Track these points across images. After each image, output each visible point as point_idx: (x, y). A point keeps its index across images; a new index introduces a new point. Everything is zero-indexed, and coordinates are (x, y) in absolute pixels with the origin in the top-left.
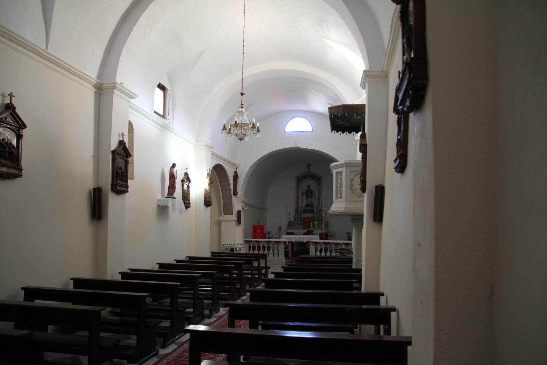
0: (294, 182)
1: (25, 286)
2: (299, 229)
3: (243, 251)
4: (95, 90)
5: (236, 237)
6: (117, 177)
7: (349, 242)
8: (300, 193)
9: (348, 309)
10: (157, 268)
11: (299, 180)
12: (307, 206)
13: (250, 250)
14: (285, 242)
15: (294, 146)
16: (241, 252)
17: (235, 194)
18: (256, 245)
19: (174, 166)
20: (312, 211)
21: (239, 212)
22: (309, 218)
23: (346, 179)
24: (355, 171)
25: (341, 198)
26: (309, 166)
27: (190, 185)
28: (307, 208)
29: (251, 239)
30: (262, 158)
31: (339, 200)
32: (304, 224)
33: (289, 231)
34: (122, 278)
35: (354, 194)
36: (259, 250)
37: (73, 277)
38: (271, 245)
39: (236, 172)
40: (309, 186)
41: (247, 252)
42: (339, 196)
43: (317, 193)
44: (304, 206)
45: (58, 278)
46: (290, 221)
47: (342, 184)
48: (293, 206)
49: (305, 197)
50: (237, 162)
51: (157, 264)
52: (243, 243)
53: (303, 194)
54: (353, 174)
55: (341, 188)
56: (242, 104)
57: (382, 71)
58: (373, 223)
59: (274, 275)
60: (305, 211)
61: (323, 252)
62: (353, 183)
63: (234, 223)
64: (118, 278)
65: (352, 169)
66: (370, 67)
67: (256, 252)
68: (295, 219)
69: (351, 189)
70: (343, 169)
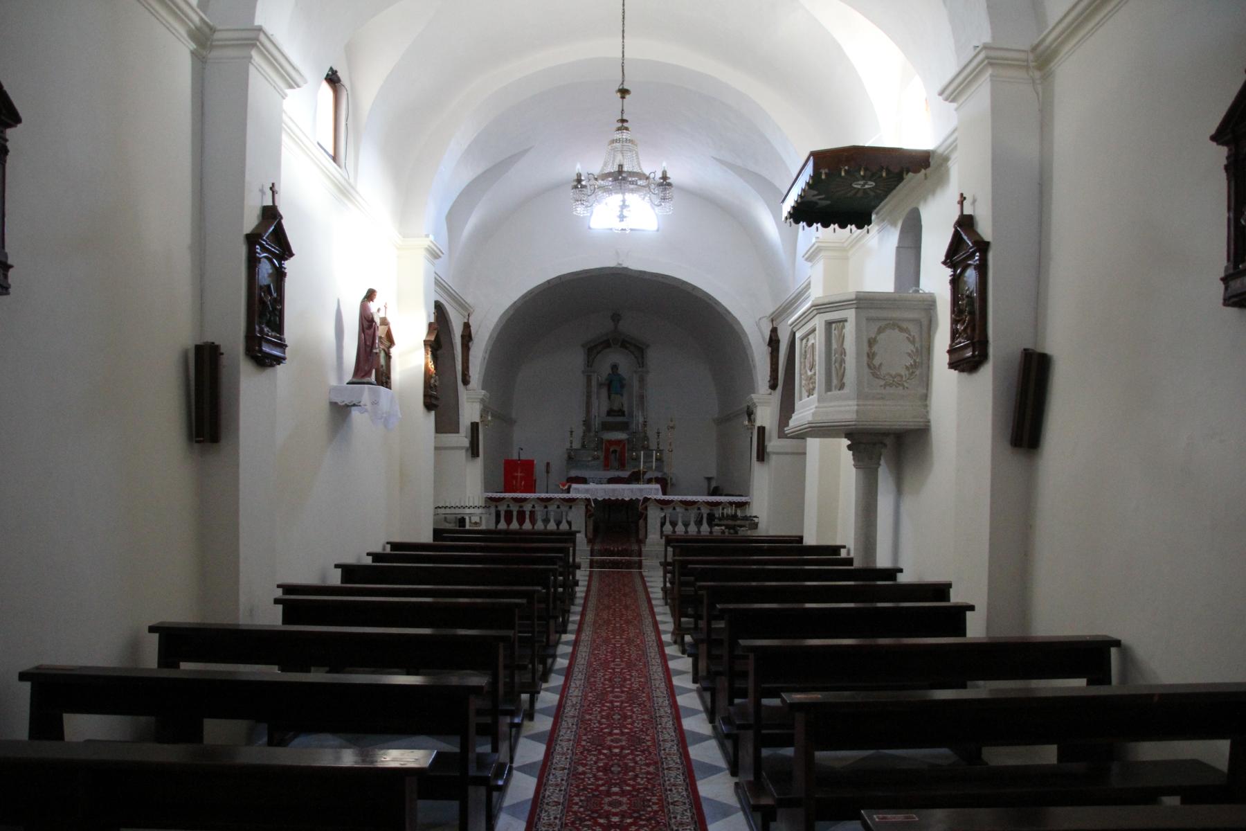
1: (27, 665)
3: (487, 523)
4: (193, 46)
5: (470, 490)
6: (262, 315)
8: (594, 383)
9: (1156, 699)
10: (335, 578)
11: (593, 350)
13: (498, 522)
14: (588, 500)
15: (612, 264)
16: (483, 527)
17: (466, 381)
18: (515, 509)
19: (370, 295)
20: (624, 427)
21: (475, 426)
22: (619, 442)
23: (858, 338)
24: (878, 319)
25: (842, 387)
26: (616, 318)
27: (393, 351)
28: (611, 419)
29: (502, 495)
31: (835, 392)
32: (606, 458)
33: (573, 473)
34: (286, 620)
35: (878, 377)
37: (153, 622)
39: (467, 326)
40: (615, 367)
41: (492, 526)
42: (835, 382)
43: (636, 384)
45: (103, 631)
46: (570, 450)
47: (843, 353)
49: (604, 392)
50: (469, 300)
51: (337, 566)
52: (482, 503)
53: (600, 385)
54: (874, 327)
55: (843, 361)
56: (623, 121)
57: (1034, 49)
60: (606, 427)
62: (875, 348)
64: (273, 618)
65: (873, 313)
66: (993, 37)
67: (515, 525)
68: (583, 446)
69: (869, 366)
70: (850, 314)
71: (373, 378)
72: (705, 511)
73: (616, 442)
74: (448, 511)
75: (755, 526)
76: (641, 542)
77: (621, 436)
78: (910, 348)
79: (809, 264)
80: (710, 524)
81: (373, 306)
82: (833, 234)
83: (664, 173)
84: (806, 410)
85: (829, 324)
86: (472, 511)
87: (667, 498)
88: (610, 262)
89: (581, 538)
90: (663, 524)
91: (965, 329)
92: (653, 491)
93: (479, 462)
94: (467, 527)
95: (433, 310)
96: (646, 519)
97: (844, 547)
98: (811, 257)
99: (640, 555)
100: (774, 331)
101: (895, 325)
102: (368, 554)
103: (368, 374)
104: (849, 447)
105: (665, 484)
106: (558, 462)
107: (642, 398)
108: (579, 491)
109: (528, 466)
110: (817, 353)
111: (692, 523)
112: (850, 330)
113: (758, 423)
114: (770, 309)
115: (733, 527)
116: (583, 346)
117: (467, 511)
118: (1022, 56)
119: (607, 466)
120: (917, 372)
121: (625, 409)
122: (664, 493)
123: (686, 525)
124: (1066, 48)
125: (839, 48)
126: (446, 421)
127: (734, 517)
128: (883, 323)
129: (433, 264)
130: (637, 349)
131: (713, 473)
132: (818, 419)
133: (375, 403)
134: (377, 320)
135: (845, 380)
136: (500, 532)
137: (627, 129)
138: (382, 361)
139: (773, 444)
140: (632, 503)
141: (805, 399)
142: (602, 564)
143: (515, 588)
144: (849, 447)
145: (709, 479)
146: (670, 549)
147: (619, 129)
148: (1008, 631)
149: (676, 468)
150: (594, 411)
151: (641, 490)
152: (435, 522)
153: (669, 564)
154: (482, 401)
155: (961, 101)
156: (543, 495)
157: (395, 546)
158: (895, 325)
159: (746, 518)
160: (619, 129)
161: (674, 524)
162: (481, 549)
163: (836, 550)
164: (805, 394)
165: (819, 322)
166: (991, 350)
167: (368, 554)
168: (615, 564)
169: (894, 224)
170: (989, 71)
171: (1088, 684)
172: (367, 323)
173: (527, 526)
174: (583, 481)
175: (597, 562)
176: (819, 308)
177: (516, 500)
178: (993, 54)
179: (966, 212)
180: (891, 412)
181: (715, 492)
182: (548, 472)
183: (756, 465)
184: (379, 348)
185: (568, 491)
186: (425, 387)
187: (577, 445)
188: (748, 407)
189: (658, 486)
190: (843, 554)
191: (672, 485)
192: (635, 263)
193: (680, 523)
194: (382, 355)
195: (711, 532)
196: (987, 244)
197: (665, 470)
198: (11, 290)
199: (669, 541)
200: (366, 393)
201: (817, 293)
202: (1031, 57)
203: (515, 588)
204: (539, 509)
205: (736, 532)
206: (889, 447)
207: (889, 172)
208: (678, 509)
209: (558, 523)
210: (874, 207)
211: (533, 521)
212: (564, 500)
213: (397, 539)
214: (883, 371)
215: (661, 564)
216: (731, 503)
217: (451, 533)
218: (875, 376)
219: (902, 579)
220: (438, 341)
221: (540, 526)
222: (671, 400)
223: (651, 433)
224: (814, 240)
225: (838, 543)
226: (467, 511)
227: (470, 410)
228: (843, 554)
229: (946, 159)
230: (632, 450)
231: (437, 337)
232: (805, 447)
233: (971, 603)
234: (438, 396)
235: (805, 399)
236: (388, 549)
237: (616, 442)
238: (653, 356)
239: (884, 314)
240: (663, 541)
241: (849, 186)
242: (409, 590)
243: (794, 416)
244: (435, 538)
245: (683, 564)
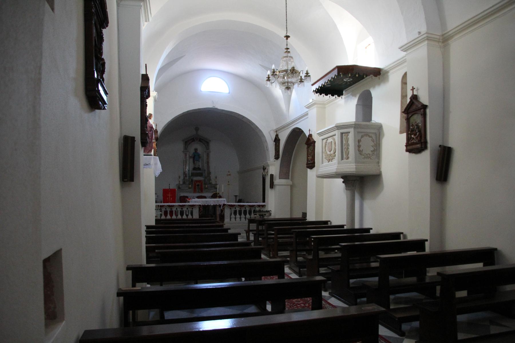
0: (181, 146)
7: (263, 204)
8: (188, 156)
11: (187, 142)
12: (194, 169)
14: (200, 205)
15: (211, 106)
18: (168, 210)
20: (201, 175)
22: (199, 181)
24: (361, 132)
25: (348, 158)
26: (197, 129)
28: (195, 171)
36: (171, 215)
38: (185, 209)
40: (196, 150)
42: (345, 156)
44: (191, 169)
47: (348, 145)
49: (191, 160)
53: (190, 157)
54: (361, 135)
55: (348, 148)
56: (287, 49)
57: (443, 35)
58: (435, 181)
61: (238, 214)
62: (360, 144)
65: (360, 130)
66: (428, 29)
67: (169, 217)
70: (352, 130)
71: (152, 153)
72: (238, 209)
75: (270, 214)
78: (372, 144)
82: (329, 97)
83: (307, 71)
85: (342, 134)
88: (210, 106)
91: (417, 138)
100: (277, 136)
101: (367, 135)
103: (151, 151)
104: (343, 182)
113: (270, 172)
114: (275, 128)
116: (183, 141)
118: (438, 37)
119: (195, 191)
120: (375, 153)
121: (200, 167)
124: (456, 37)
125: (335, 26)
127: (260, 211)
128: (363, 134)
130: (206, 142)
132: (339, 171)
137: (289, 52)
143: (198, 244)
144: (343, 182)
145: (236, 196)
147: (286, 52)
148: (437, 249)
155: (409, 52)
158: (367, 135)
160: (286, 52)
166: (429, 145)
169: (354, 95)
170: (426, 42)
171: (484, 265)
173: (185, 217)
177: (169, 206)
178: (430, 36)
179: (415, 93)
180: (367, 169)
181: (240, 201)
187: (181, 183)
192: (220, 106)
196: (425, 107)
202: (441, 38)
203: (198, 244)
206: (361, 183)
207: (359, 74)
210: (345, 89)
211: (177, 215)
214: (364, 152)
218: (361, 154)
219: (372, 232)
222: (222, 163)
229: (387, 72)
230: (205, 184)
233: (426, 239)
238: (212, 145)
239: (363, 130)
241: (345, 80)
242: (215, 245)
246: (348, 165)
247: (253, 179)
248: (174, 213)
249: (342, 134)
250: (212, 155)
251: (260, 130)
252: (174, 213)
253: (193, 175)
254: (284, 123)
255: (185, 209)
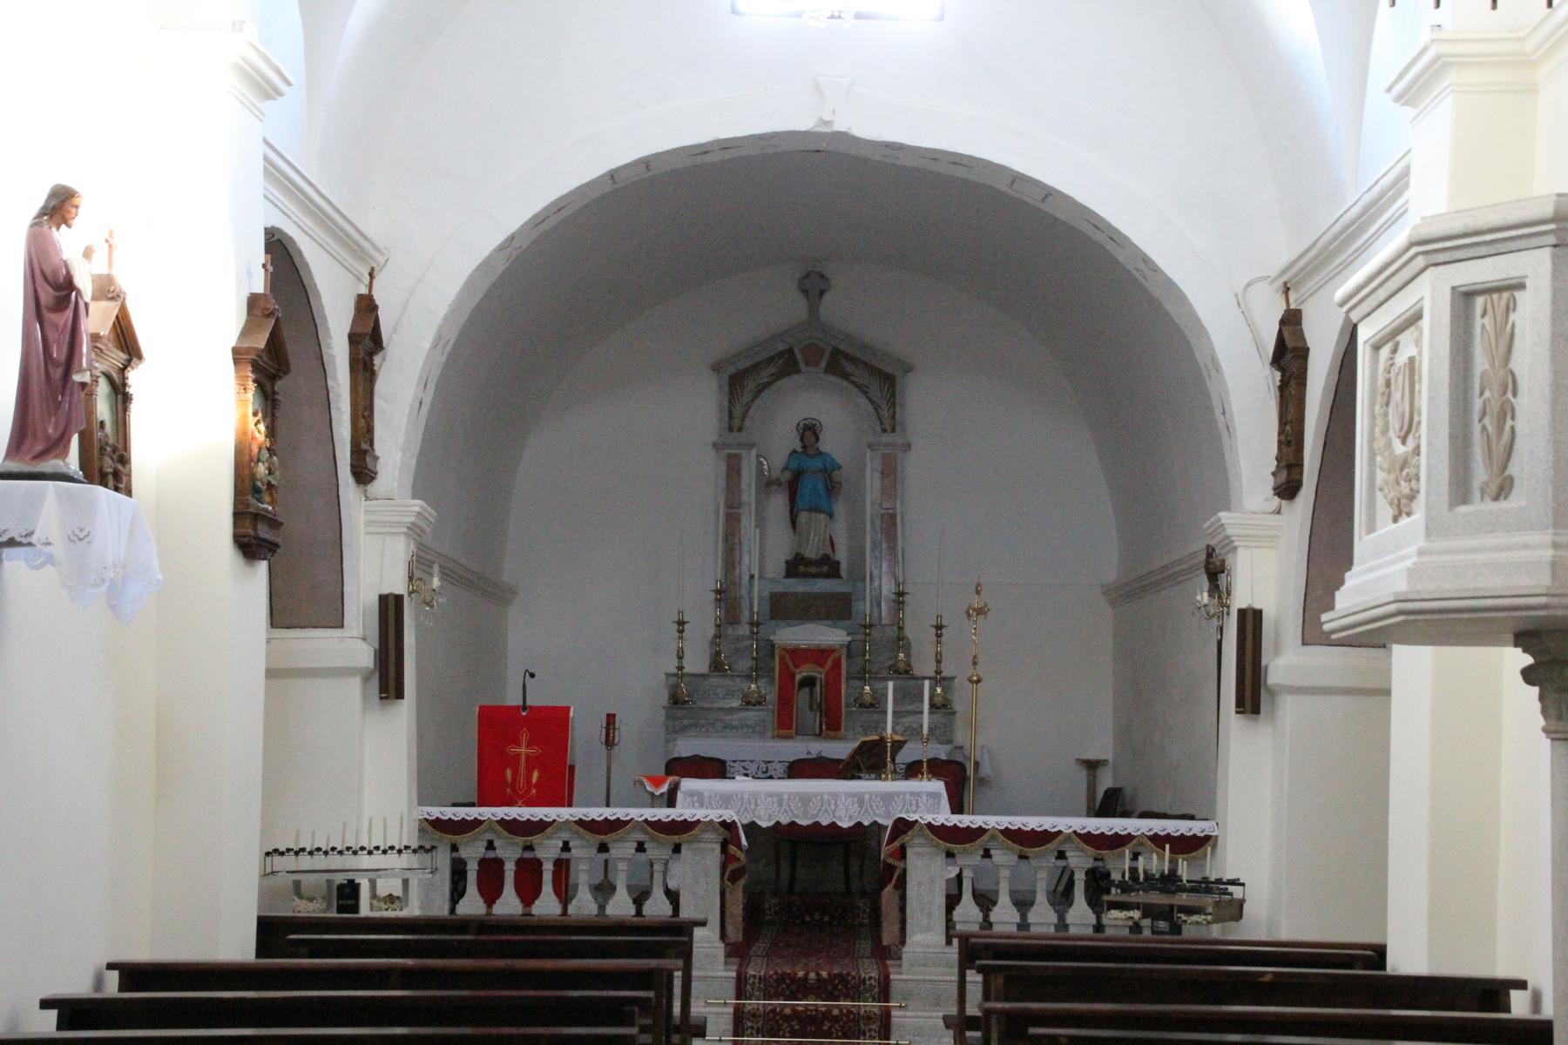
0: (698, 406)
2: (756, 731)
3: (424, 898)
5: (372, 801)
11: (747, 380)
12: (796, 566)
13: (457, 893)
14: (729, 826)
15: (801, 121)
16: (413, 909)
17: (363, 473)
18: (509, 852)
19: (59, 207)
20: (837, 609)
21: (390, 608)
22: (819, 655)
25: (1503, 490)
26: (814, 285)
27: (136, 379)
28: (798, 586)
30: (558, 206)
31: (1481, 507)
33: (687, 747)
36: (529, 889)
39: (366, 307)
40: (809, 431)
41: (440, 909)
42: (1480, 474)
43: (872, 484)
47: (1510, 385)
48: (703, 576)
49: (778, 503)
50: (373, 225)
53: (767, 484)
55: (1506, 412)
59: (52, 1015)
60: (783, 608)
63: (353, 692)
67: (509, 904)
68: (717, 666)
70: (1535, 266)
71: (72, 461)
72: (1079, 861)
73: (812, 657)
74: (305, 862)
75: (1236, 910)
76: (886, 954)
77: (829, 635)
79: (1409, 112)
80: (1094, 902)
81: (68, 243)
84: (1390, 559)
85: (1465, 297)
86: (378, 861)
87: (964, 820)
89: (707, 942)
90: (952, 901)
92: (925, 800)
93: (404, 712)
94: (365, 911)
95: (260, 256)
96: (901, 885)
97: (1521, 985)
98: (1413, 90)
99: (884, 992)
100: (1291, 319)
102: (46, 1004)
103: (57, 446)
104: (1528, 675)
105: (957, 778)
106: (641, 705)
107: (890, 523)
108: (701, 800)
109: (550, 726)
110: (1424, 387)
111: (1041, 898)
112: (1532, 315)
113: (1241, 599)
114: (1280, 253)
115: (1167, 913)
116: (716, 368)
117: (365, 861)
119: (785, 724)
121: (842, 556)
122: (957, 808)
123: (1023, 903)
126: (303, 597)
127: (1169, 881)
129: (260, 116)
130: (877, 379)
131: (1102, 748)
132: (1428, 587)
133: (79, 537)
134: (84, 283)
135: (1513, 469)
136: (463, 925)
138: (103, 409)
139: (1285, 661)
140: (859, 838)
141: (1386, 528)
142: (772, 1024)
144: (1528, 675)
145: (1092, 766)
146: (974, 977)
149: (997, 730)
150: (749, 562)
151: (887, 798)
152: (265, 895)
153: (972, 1023)
154: (414, 530)
156: (597, 813)
157: (133, 975)
159: (1204, 886)
161: (986, 901)
162: (407, 978)
163: (1493, 992)
164: (1384, 511)
165: (1432, 293)
167: (46, 1004)
168: (810, 1024)
172: (52, 294)
174: (714, 768)
175: (754, 1015)
176: (1436, 249)
177: (512, 827)
181: (1111, 804)
182: (609, 742)
183: (1233, 723)
184: (91, 368)
185: (671, 801)
186: (239, 491)
187: (696, 662)
188: (1210, 551)
189: (938, 786)
190: (1519, 1007)
191: (982, 782)
193: (1004, 899)
194: (103, 389)
195: (1099, 927)
197: (961, 737)
198: (1257, 606)
199: (972, 952)
200: (49, 506)
201: (1430, 204)
204: (583, 853)
205: (1176, 929)
208: (999, 856)
209: (640, 898)
211: (564, 892)
212: (658, 826)
213: (142, 952)
215: (948, 1022)
216: (1158, 840)
217: (314, 943)
220: (278, 348)
221: (584, 905)
222: (978, 532)
223: (918, 630)
224: (1425, 36)
225: (1502, 972)
226: (365, 861)
227: (377, 551)
228: (1519, 1007)
230: (862, 675)
231: (275, 341)
232: (1387, 673)
234: (273, 521)
235: (1386, 528)
236: (112, 986)
237: (812, 657)
238: (922, 399)
240: (953, 952)
243: (1352, 579)
244: (263, 949)
245: (1015, 1024)
246: (1502, 539)
247: (1186, 648)
248: (547, 877)
249: (1465, 297)
250: (915, 468)
251: (1170, 285)
252: (547, 877)
253: (783, 608)
254: (1355, 196)
255: (623, 850)
